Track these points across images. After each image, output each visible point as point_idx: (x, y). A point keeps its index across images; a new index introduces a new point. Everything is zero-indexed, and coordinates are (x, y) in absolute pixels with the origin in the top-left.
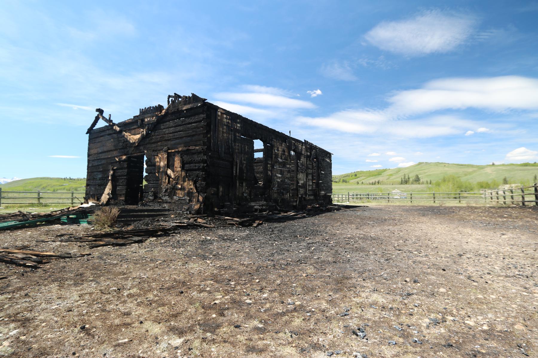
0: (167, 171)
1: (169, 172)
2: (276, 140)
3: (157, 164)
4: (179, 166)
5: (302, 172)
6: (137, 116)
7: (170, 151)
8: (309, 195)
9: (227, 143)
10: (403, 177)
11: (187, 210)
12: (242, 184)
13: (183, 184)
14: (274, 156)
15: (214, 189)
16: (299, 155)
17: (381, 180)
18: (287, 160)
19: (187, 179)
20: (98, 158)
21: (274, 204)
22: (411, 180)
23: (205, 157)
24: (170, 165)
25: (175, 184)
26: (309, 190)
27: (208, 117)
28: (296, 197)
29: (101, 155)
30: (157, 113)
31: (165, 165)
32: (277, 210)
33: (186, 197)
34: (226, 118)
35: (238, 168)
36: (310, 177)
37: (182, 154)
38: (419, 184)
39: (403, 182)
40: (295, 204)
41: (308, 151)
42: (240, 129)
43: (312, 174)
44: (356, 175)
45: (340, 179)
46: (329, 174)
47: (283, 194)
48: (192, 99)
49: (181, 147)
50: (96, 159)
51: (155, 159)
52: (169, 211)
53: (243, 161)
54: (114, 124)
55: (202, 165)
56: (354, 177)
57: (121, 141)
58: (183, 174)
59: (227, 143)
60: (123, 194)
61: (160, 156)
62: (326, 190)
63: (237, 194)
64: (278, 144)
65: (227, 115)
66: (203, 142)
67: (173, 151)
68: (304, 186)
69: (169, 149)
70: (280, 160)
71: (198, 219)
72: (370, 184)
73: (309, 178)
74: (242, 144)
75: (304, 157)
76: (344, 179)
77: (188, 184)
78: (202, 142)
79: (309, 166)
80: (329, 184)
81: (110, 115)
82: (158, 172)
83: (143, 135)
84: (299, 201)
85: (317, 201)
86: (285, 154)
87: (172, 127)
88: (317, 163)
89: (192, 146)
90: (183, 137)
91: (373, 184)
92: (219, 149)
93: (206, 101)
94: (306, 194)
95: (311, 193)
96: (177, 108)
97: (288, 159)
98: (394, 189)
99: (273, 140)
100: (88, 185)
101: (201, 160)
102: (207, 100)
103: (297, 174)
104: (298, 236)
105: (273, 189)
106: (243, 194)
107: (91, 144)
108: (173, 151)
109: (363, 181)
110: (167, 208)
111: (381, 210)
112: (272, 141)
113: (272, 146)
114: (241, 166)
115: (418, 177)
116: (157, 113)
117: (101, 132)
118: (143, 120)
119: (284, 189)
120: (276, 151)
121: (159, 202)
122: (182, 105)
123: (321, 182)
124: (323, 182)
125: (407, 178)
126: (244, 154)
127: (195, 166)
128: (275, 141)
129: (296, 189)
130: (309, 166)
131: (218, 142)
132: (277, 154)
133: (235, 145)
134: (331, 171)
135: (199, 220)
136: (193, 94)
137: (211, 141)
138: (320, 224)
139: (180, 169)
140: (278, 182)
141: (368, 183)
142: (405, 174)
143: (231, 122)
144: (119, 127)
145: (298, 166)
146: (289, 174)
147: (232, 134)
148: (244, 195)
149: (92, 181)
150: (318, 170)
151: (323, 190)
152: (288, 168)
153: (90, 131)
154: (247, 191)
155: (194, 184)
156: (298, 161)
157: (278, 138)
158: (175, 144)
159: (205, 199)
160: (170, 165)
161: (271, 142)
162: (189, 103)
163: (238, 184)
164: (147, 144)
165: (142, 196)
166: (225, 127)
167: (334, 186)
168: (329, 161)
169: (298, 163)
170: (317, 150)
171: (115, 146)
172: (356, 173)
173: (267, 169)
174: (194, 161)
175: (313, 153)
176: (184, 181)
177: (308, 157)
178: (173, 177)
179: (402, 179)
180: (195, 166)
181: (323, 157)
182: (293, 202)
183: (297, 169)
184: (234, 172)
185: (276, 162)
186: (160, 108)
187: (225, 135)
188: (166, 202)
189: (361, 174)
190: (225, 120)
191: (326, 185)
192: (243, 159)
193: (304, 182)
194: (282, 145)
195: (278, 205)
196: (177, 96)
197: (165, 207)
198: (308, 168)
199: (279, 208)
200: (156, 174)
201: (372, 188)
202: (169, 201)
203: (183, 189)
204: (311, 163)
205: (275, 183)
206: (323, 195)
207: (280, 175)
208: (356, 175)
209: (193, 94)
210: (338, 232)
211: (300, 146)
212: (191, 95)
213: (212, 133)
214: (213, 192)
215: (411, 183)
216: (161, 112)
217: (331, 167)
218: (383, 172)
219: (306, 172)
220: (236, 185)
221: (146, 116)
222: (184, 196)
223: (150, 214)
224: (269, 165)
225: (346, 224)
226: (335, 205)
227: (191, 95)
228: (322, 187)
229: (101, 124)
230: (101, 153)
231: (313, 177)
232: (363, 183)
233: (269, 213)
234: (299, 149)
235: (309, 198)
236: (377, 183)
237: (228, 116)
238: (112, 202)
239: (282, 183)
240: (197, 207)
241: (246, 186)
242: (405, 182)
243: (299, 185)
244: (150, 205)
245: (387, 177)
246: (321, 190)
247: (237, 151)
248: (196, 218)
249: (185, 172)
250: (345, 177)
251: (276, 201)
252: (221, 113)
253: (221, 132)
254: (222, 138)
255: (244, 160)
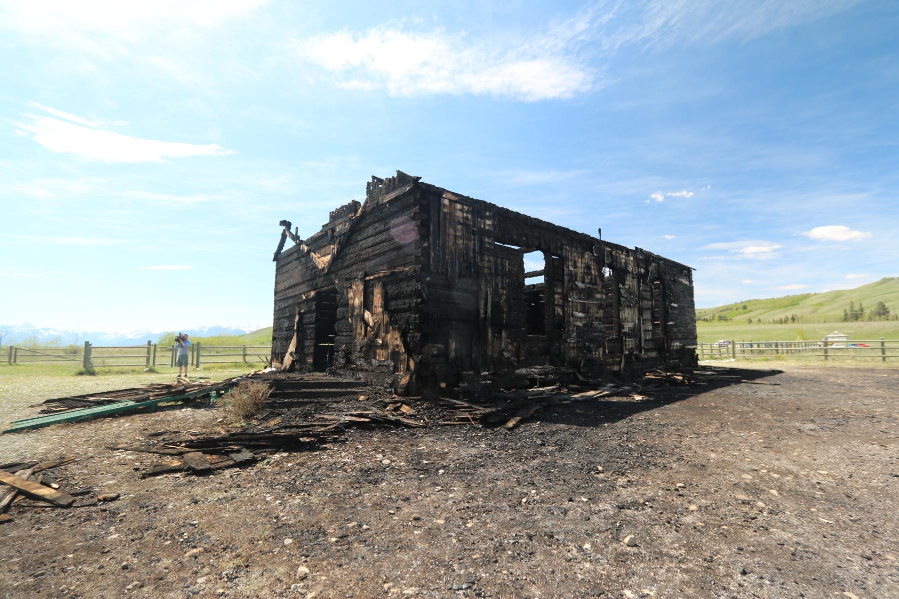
0: (363, 314)
1: (367, 315)
2: (571, 247)
3: (351, 302)
4: (380, 305)
5: (629, 306)
6: (327, 225)
7: (367, 278)
8: (647, 350)
9: (465, 256)
10: (848, 308)
11: (391, 386)
12: (501, 334)
13: (386, 336)
14: (566, 278)
15: (439, 346)
16: (620, 273)
17: (799, 315)
18: (596, 284)
19: (391, 328)
20: (285, 297)
21: (570, 371)
22: (867, 312)
23: (419, 286)
26: (646, 340)
27: (424, 209)
28: (619, 355)
29: (287, 292)
30: (350, 216)
31: (361, 302)
32: (575, 381)
34: (462, 210)
35: (489, 304)
36: (647, 315)
37: (385, 283)
38: (887, 320)
39: (849, 316)
40: (616, 368)
41: (641, 265)
42: (492, 229)
43: (652, 309)
44: (745, 308)
45: (714, 315)
46: (689, 307)
47: (589, 350)
48: (397, 180)
49: (383, 270)
50: (282, 298)
51: (347, 293)
52: (366, 386)
53: (501, 291)
54: (302, 242)
55: (415, 300)
56: (741, 310)
57: (309, 267)
58: (386, 318)
59: (465, 256)
60: (311, 354)
61: (354, 287)
62: (683, 339)
63: (490, 353)
64: (575, 254)
65: (463, 204)
66: (415, 256)
67: (372, 277)
68: (635, 333)
69: (366, 275)
70: (580, 285)
71: (404, 405)
72: (775, 322)
73: (645, 317)
74: (497, 257)
75: (633, 278)
76: (722, 314)
77: (392, 337)
78: (413, 257)
79: (644, 293)
80: (689, 327)
81: (297, 228)
82: (352, 316)
83: (333, 254)
84: (626, 362)
85: (665, 360)
86: (591, 274)
87: (371, 236)
88: (661, 287)
89: (399, 266)
90: (386, 252)
91: (781, 322)
92: (448, 269)
93: (420, 181)
94: (639, 347)
95: (651, 345)
96: (376, 201)
97: (599, 282)
98: (831, 330)
99: (565, 247)
100: (274, 339)
101: (412, 291)
102: (421, 178)
103: (619, 311)
104: (600, 468)
105: (567, 342)
106: (501, 353)
107: (279, 276)
108: (372, 277)
109: (761, 317)
110: (363, 380)
111: (815, 380)
112: (561, 249)
113: (563, 260)
114: (497, 300)
115: (884, 306)
116: (350, 216)
117: (289, 256)
118: (333, 230)
119: (591, 341)
120: (571, 268)
121: (352, 369)
122: (383, 195)
123: (671, 323)
124: (676, 324)
125: (857, 308)
126: (503, 276)
127: (404, 304)
128: (568, 248)
129: (617, 339)
130: (644, 293)
131: (444, 256)
132: (573, 273)
133: (482, 260)
134: (692, 301)
135: (405, 409)
136: (399, 173)
137: (429, 254)
138: (664, 425)
139: (381, 310)
140: (578, 327)
141: (771, 320)
142: (852, 302)
143: (473, 216)
144: (307, 245)
145: (619, 295)
146: (601, 311)
147: (474, 240)
148: (504, 356)
149: (278, 333)
150: (665, 302)
151: (678, 339)
152: (598, 300)
153: (277, 257)
154: (510, 347)
155: (401, 337)
156: (621, 286)
157: (575, 244)
158: (375, 265)
159: (418, 365)
160: (367, 304)
161: (559, 252)
163: (490, 335)
164: (339, 270)
165: (331, 359)
166: (459, 227)
167: (701, 329)
168: (687, 283)
169: (619, 289)
170: (661, 262)
171: (302, 276)
172: (746, 304)
173: (554, 303)
174: (403, 293)
175: (651, 268)
176: (387, 332)
177: (640, 277)
178: (371, 324)
179: (845, 311)
181: (674, 275)
182: (613, 364)
183: (619, 301)
184: (482, 311)
185: (572, 290)
186: (355, 204)
187: (460, 242)
188: (362, 370)
189: (755, 304)
190: (459, 214)
191: (682, 329)
192: (500, 285)
193: (634, 325)
194: (583, 257)
195: (580, 373)
196: (377, 181)
197: (359, 379)
198: (641, 298)
199: (581, 378)
200: (348, 319)
201: (779, 329)
203: (384, 346)
204: (648, 289)
205: (571, 329)
206: (677, 350)
207: (581, 315)
208: (745, 308)
209: (399, 171)
210: (713, 455)
211: (623, 256)
212: (395, 175)
213: (431, 239)
214: (436, 352)
215: (867, 318)
216: (356, 212)
217: (691, 295)
218: (802, 300)
219: (638, 306)
220: (487, 336)
221: (336, 222)
222: (386, 360)
223: (330, 392)
224: (556, 296)
225: (734, 429)
226: (705, 368)
227: (395, 175)
228: (675, 332)
229: (290, 244)
230: (288, 289)
231: (653, 314)
232: (760, 321)
233: (559, 389)
234: (621, 263)
235: (646, 356)
236: (790, 321)
237: (465, 207)
239: (586, 329)
240: (404, 381)
241: (508, 337)
242: (856, 316)
243: (623, 331)
244: (340, 374)
245: (812, 308)
246: (672, 340)
247: (486, 270)
248: (399, 404)
249: (388, 314)
250: (724, 311)
251: (575, 364)
252: (450, 201)
253: (452, 237)
254: (453, 248)
255: (503, 288)
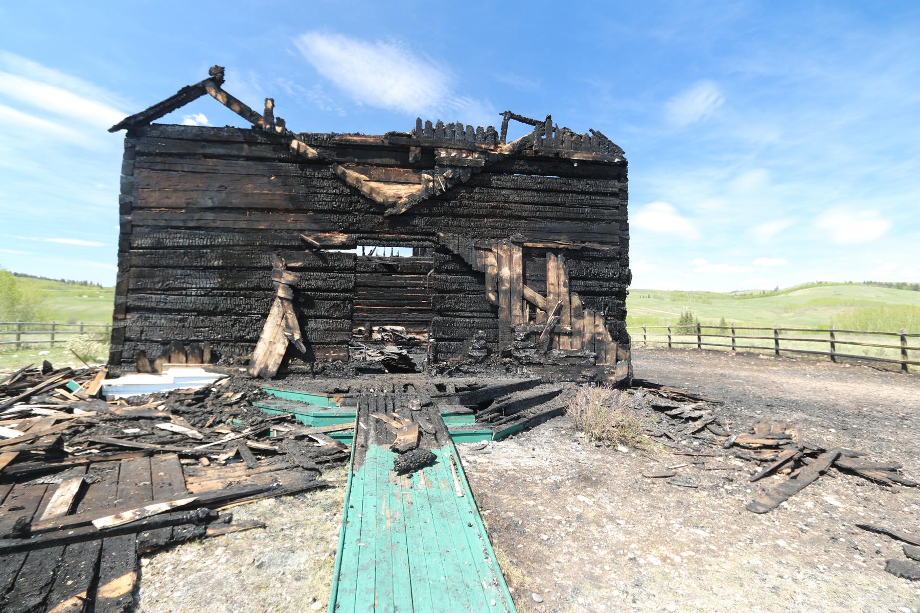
24: (537, 278)
25: (555, 322)
33: (587, 352)
139: (566, 290)
162: (588, 150)
180: (601, 286)
202: (538, 360)
238: (299, 364)
